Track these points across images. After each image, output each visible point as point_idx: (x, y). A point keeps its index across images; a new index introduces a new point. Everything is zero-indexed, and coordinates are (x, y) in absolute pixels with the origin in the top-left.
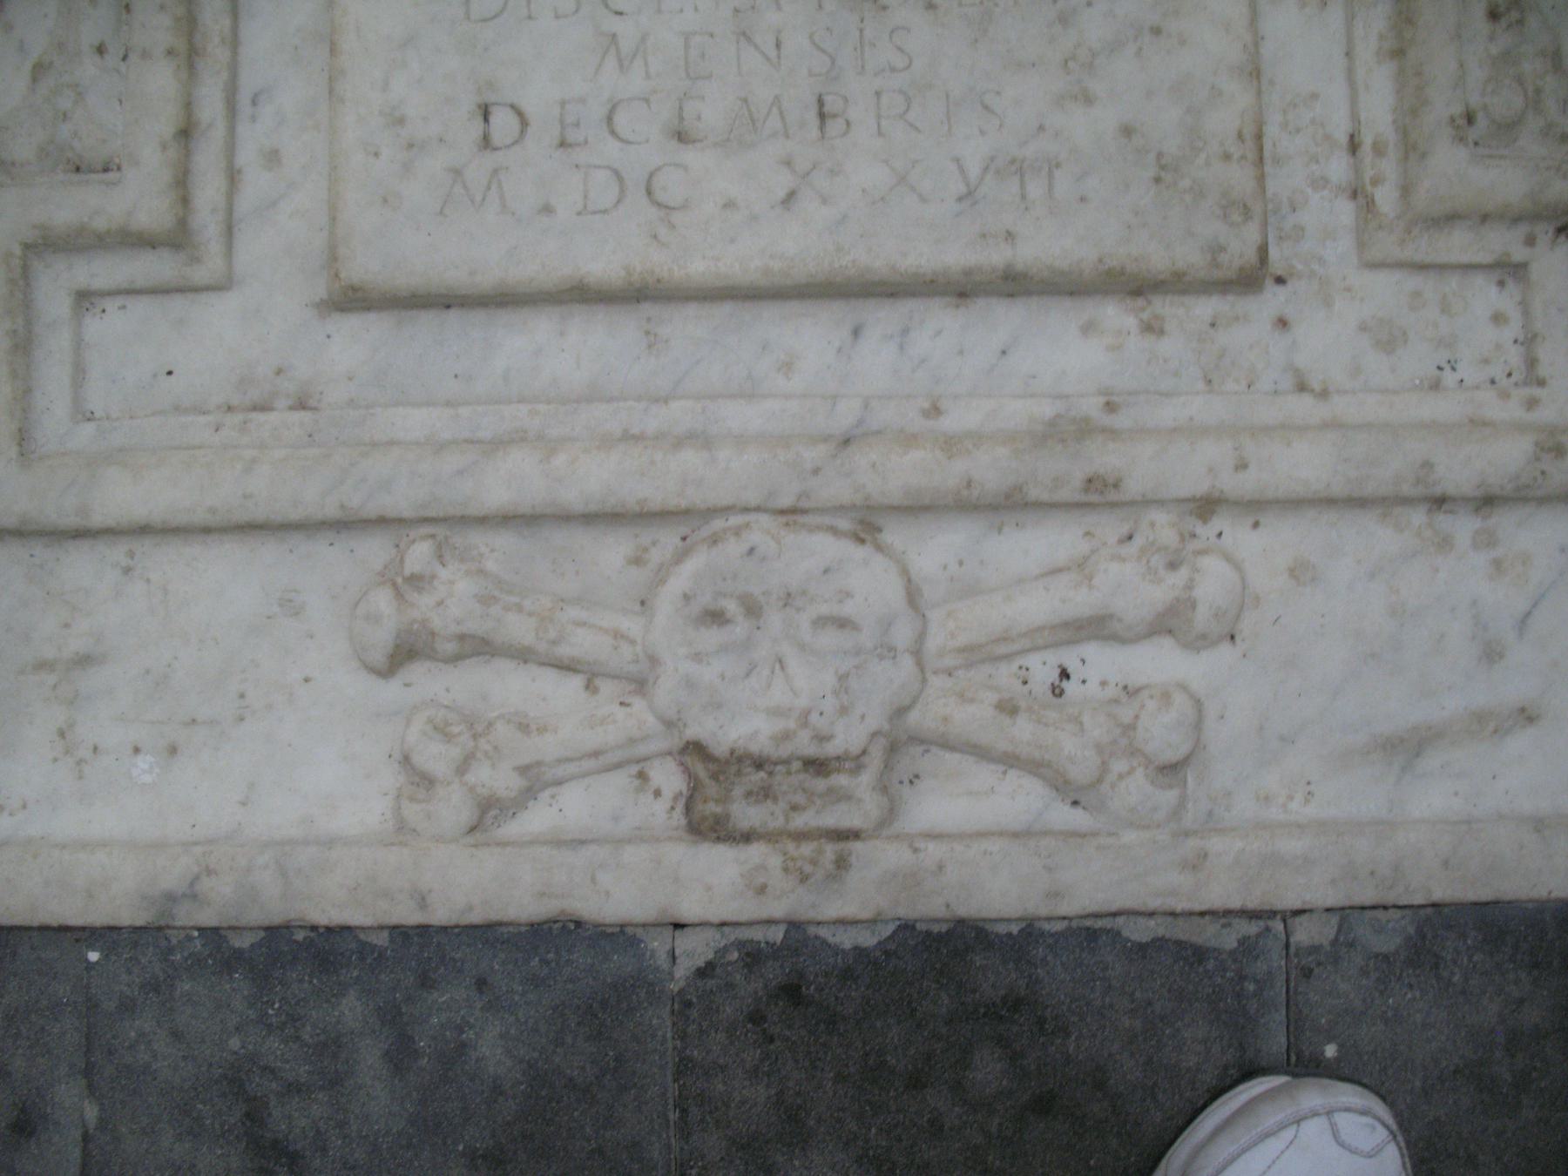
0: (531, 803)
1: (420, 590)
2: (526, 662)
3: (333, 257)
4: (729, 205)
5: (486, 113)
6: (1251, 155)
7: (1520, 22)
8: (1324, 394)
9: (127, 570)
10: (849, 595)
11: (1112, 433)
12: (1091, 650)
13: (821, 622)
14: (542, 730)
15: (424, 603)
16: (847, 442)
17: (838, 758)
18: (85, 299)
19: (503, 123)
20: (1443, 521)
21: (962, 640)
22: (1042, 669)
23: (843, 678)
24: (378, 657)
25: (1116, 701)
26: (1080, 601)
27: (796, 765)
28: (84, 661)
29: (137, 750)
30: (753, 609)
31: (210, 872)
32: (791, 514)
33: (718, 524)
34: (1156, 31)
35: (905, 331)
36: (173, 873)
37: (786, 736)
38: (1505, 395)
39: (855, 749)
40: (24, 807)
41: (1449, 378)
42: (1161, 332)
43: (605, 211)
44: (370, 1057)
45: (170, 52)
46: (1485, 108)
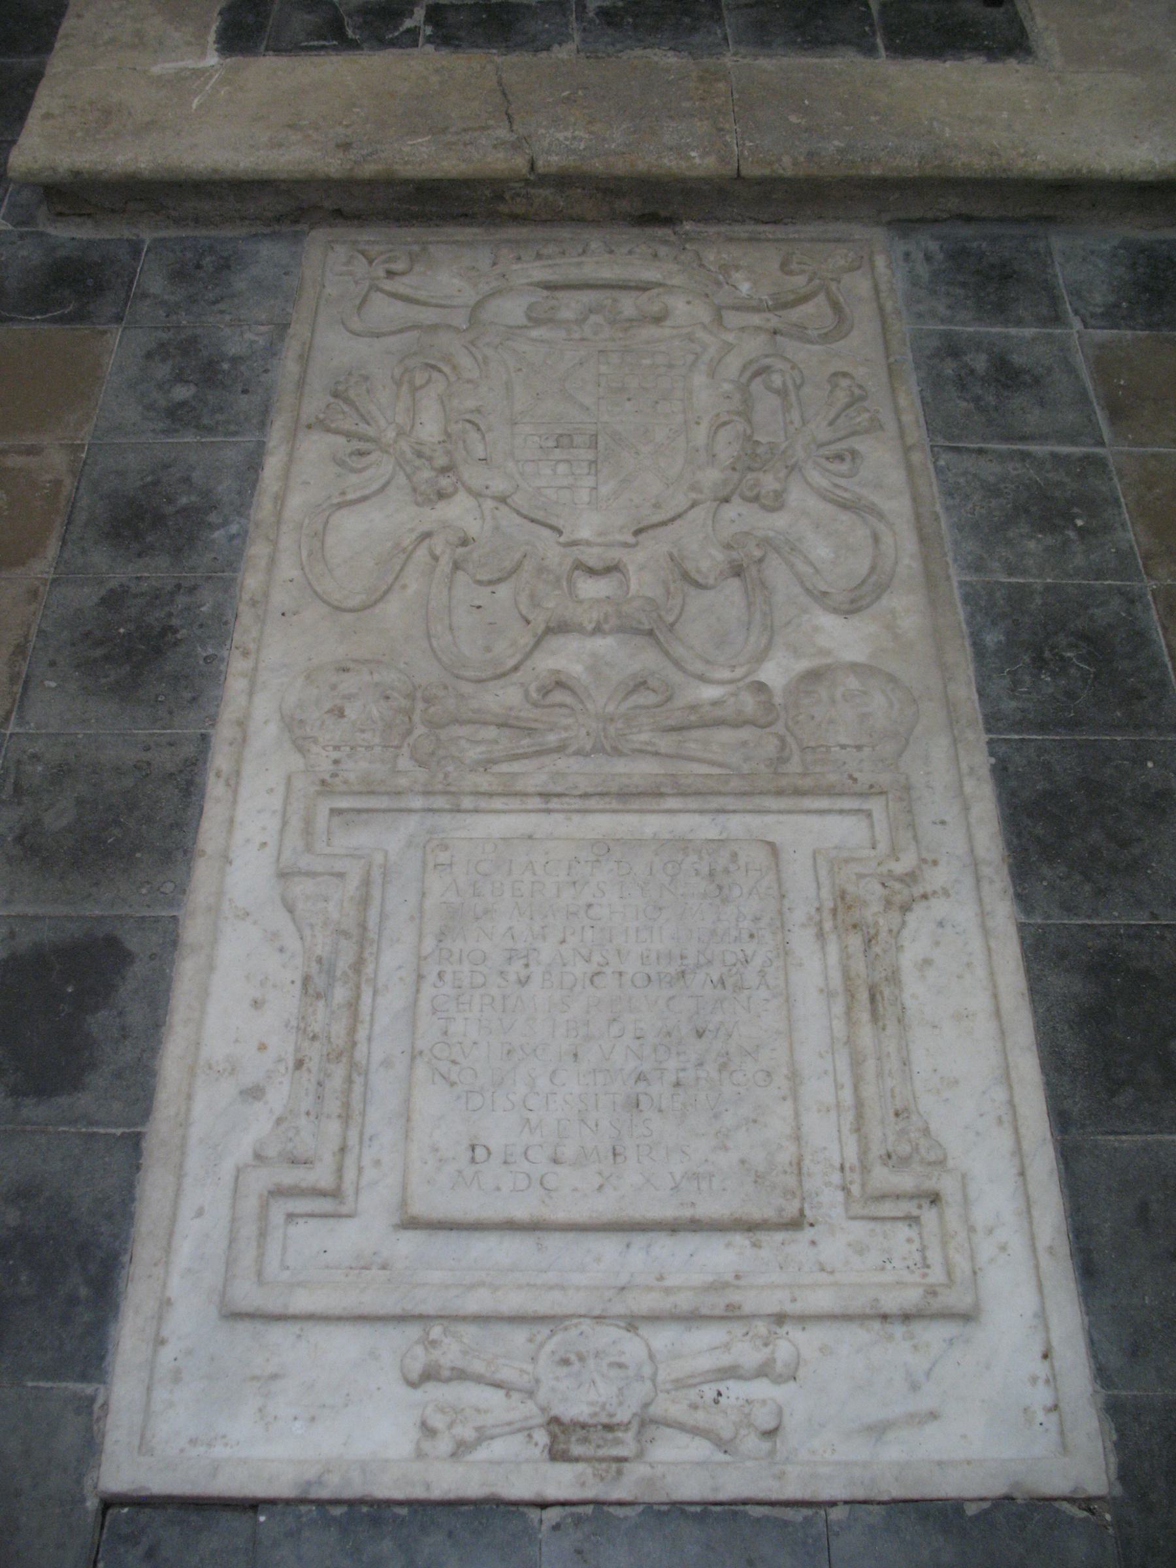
0: (479, 1448)
1: (434, 1348)
2: (479, 1383)
3: (404, 1203)
4: (576, 1190)
5: (473, 1148)
6: (796, 1172)
7: (908, 1117)
8: (832, 1272)
9: (299, 1336)
10: (624, 1353)
11: (738, 1287)
12: (731, 1383)
13: (611, 1365)
14: (486, 1412)
15: (436, 1354)
16: (623, 1288)
17: (618, 1424)
18: (291, 1217)
19: (480, 1153)
20: (889, 1328)
21: (673, 1376)
22: (709, 1391)
23: (620, 1389)
24: (414, 1376)
25: (743, 1406)
26: (725, 1360)
27: (600, 1427)
28: (275, 1377)
29: (295, 1419)
30: (581, 1358)
31: (329, 1471)
32: (599, 1318)
33: (567, 1323)
34: (755, 1121)
35: (649, 1246)
36: (311, 1473)
37: (595, 1414)
38: (913, 1272)
39: (626, 1420)
40: (238, 1443)
41: (888, 1266)
42: (760, 1247)
43: (522, 1191)
45: (339, 1116)
46: (895, 1151)
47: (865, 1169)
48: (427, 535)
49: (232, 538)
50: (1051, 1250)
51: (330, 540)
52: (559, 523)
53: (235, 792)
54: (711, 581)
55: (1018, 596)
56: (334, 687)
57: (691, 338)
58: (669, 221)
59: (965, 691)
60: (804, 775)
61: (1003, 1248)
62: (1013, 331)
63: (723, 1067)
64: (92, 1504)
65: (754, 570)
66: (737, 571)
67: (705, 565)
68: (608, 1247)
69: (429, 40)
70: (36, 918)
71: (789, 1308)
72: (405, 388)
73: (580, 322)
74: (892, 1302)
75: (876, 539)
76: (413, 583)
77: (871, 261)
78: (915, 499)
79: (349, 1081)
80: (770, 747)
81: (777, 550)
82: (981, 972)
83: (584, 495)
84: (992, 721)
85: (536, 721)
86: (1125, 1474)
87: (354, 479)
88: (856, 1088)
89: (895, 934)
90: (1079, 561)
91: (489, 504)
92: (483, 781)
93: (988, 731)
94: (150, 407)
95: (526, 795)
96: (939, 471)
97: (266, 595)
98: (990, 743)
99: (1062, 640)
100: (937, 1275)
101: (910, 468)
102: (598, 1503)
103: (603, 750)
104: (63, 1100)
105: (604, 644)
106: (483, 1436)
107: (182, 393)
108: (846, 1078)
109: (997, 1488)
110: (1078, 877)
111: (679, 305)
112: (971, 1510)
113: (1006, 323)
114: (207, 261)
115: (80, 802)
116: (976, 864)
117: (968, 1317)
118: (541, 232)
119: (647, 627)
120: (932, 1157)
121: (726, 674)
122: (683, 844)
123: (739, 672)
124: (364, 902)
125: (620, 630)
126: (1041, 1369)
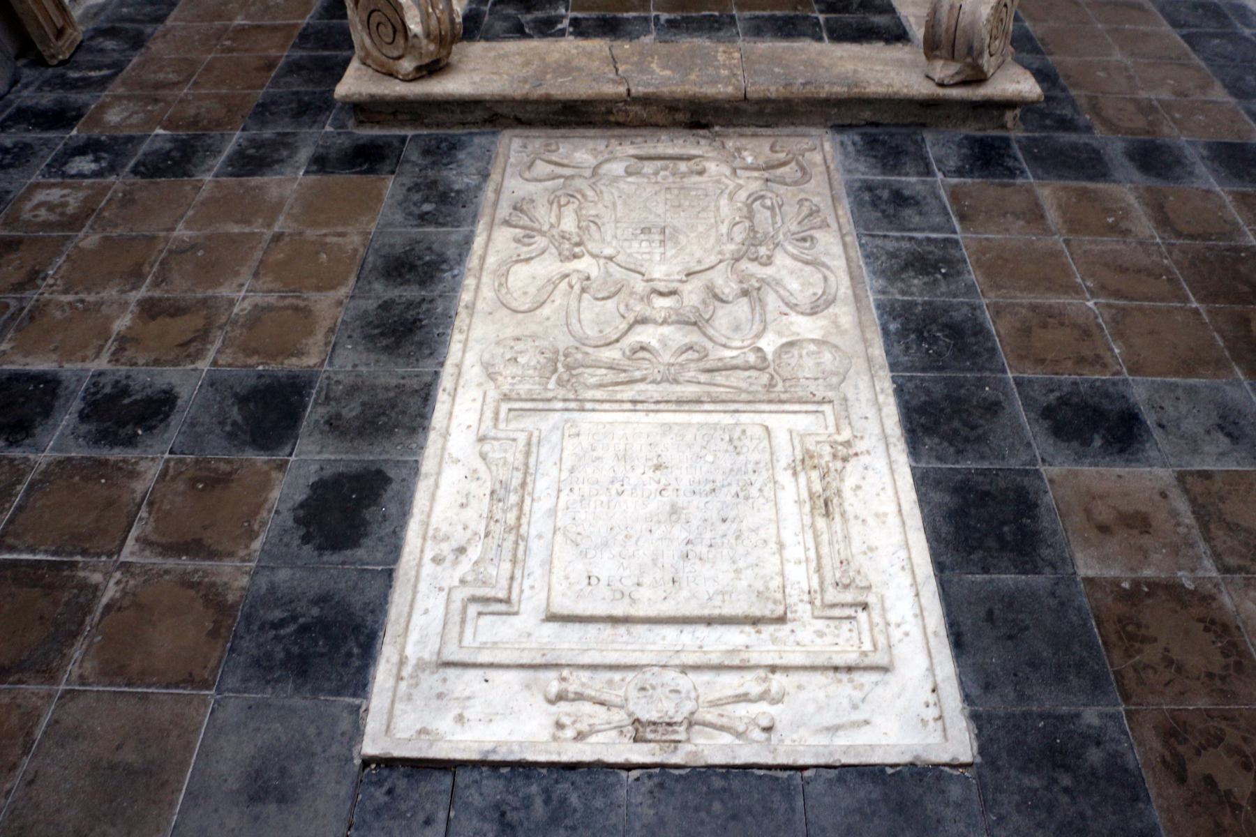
18: (480, 614)
19: (594, 581)
28: (469, 698)
30: (653, 688)
32: (664, 666)
36: (489, 747)
44: (539, 801)
47: (822, 590)
48: (567, 276)
49: (454, 276)
50: (935, 633)
51: (511, 278)
52: (643, 270)
53: (454, 399)
54: (730, 299)
55: (908, 307)
56: (512, 348)
57: (719, 182)
58: (706, 126)
59: (878, 351)
60: (786, 392)
61: (907, 634)
62: (903, 179)
63: (737, 538)
64: (357, 761)
65: (755, 293)
66: (745, 293)
67: (727, 291)
68: (670, 632)
69: (571, 34)
70: (335, 461)
71: (778, 662)
72: (555, 206)
73: (656, 173)
74: (839, 660)
75: (826, 279)
76: (558, 297)
77: (822, 146)
78: (848, 259)
79: (516, 543)
80: (765, 378)
81: (768, 284)
82: (890, 492)
83: (657, 257)
84: (893, 366)
85: (843, 514)
86: (982, 751)
87: (526, 249)
88: (817, 549)
89: (840, 472)
90: (943, 289)
91: (602, 261)
92: (599, 394)
93: (892, 371)
94: (411, 214)
95: (622, 401)
96: (861, 245)
97: (474, 304)
98: (893, 377)
99: (934, 327)
100: (867, 646)
101: (845, 245)
102: (663, 766)
103: (668, 381)
104: (348, 552)
105: (666, 330)
106: (593, 731)
107: (427, 207)
108: (811, 544)
109: (906, 759)
110: (946, 444)
111: (712, 167)
112: (890, 771)
113: (899, 174)
114: (444, 145)
115: (363, 404)
116: (885, 437)
117: (885, 669)
118: (633, 132)
119: (693, 320)
120: (863, 584)
121: (739, 344)
122: (715, 426)
123: (746, 343)
124: (528, 454)
125: (678, 322)
126: (932, 698)
